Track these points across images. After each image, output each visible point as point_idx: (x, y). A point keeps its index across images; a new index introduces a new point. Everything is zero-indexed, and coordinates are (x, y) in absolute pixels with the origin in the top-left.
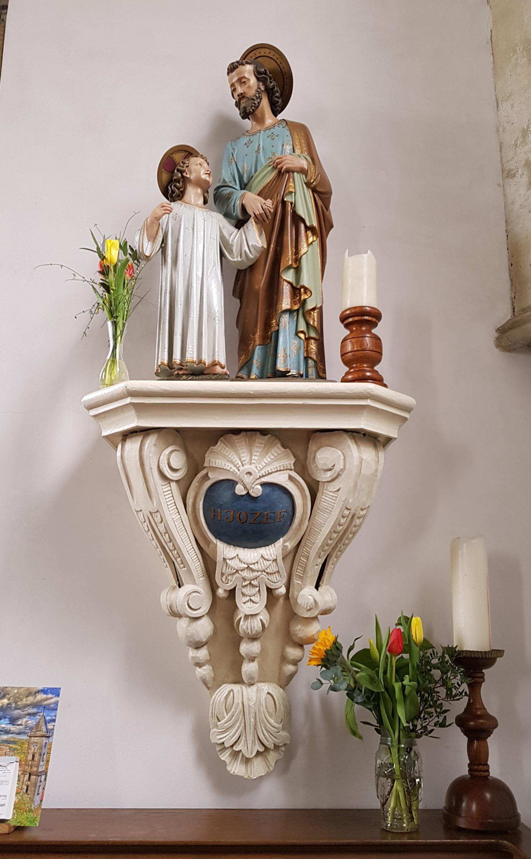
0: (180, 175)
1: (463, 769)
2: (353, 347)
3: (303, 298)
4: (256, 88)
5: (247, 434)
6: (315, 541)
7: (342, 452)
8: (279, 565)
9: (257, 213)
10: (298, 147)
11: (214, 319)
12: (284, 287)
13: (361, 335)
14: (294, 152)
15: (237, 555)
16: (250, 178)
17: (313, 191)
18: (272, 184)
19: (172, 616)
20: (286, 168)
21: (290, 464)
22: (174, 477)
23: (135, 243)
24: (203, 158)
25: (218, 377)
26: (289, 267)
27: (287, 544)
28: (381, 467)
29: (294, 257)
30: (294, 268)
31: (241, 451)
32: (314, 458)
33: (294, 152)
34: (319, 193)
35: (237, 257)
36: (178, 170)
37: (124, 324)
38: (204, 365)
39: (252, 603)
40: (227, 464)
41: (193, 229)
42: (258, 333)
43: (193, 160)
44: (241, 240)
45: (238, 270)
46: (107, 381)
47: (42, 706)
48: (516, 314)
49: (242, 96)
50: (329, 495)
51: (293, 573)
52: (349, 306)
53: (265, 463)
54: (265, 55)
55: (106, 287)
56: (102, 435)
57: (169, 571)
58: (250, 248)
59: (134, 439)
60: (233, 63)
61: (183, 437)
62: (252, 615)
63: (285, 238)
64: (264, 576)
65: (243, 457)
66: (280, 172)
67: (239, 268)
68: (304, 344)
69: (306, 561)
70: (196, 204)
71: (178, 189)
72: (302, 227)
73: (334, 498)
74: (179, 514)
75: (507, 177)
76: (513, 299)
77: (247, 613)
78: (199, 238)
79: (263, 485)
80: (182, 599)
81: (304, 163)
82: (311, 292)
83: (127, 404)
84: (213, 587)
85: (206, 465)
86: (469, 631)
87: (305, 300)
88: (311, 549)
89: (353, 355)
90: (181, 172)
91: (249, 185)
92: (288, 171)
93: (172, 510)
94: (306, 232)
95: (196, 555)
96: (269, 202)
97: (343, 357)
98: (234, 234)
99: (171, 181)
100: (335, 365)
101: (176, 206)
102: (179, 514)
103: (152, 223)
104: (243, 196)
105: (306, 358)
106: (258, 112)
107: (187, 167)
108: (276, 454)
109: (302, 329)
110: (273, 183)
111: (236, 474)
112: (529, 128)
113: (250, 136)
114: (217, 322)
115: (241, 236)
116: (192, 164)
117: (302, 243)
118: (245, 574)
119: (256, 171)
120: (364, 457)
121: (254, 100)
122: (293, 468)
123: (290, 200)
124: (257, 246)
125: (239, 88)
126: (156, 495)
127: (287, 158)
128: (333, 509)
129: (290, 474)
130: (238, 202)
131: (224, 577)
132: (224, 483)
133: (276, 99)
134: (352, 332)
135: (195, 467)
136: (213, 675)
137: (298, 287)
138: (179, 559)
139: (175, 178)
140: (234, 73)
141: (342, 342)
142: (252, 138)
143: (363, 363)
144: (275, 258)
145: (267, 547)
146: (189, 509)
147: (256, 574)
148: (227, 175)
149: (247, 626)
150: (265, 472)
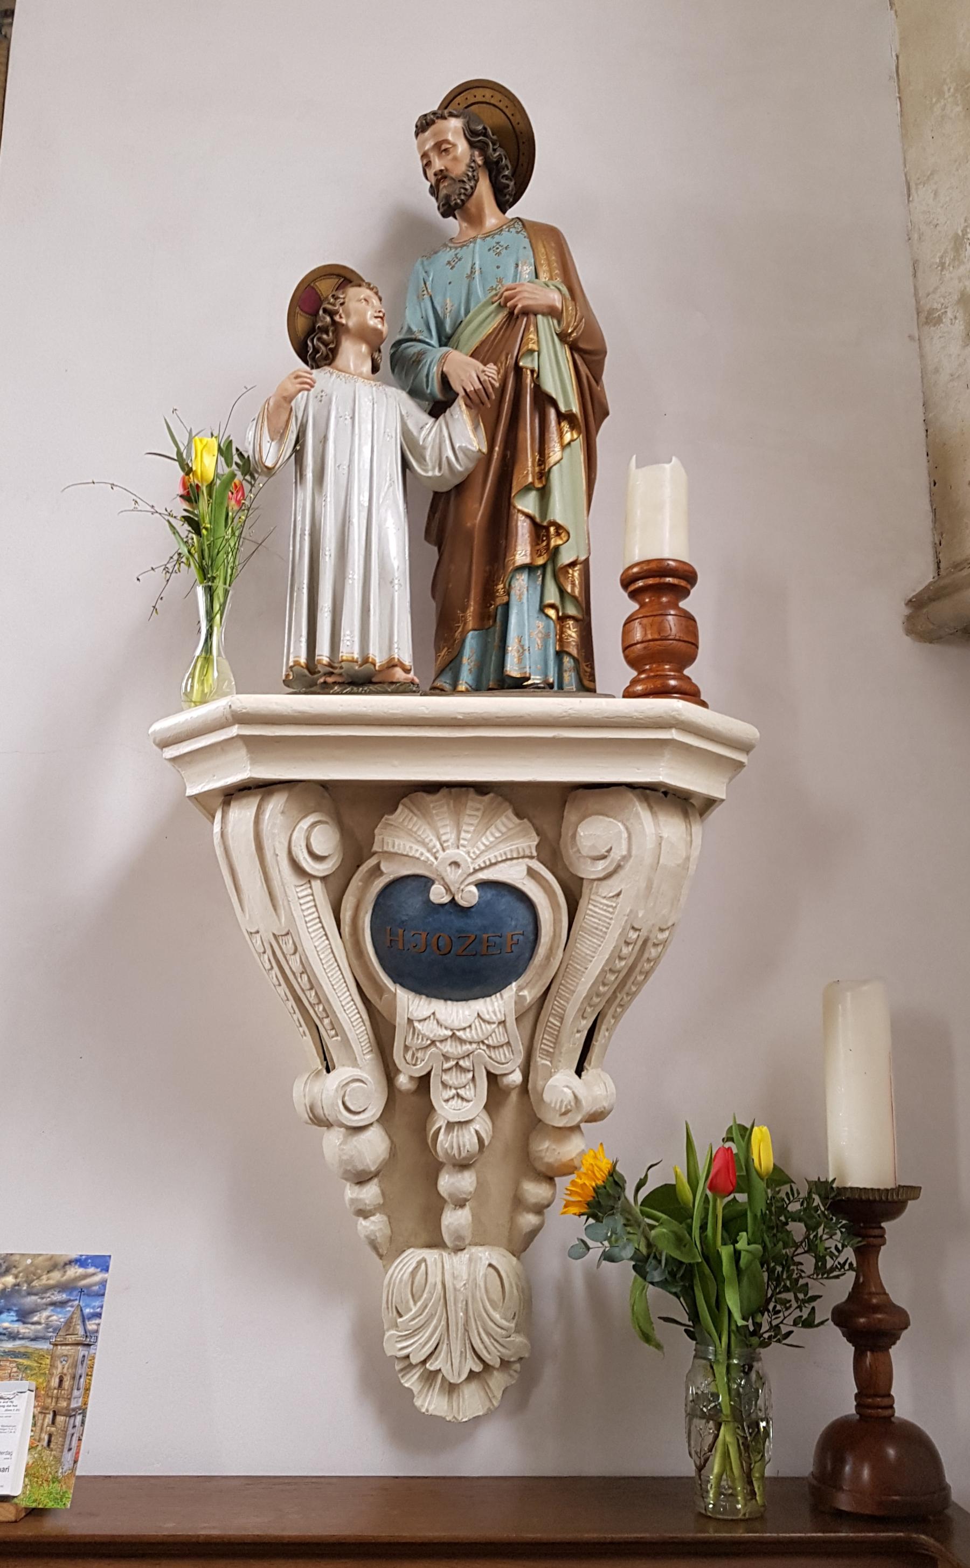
0: (328, 319)
1: (845, 1405)
2: (646, 634)
3: (553, 544)
4: (467, 160)
5: (450, 792)
6: (576, 987)
7: (624, 825)
8: (509, 1031)
9: (470, 388)
10: (545, 268)
11: (391, 582)
12: (519, 523)
13: (660, 612)
14: (537, 277)
15: (434, 1014)
16: (457, 325)
17: (571, 349)
18: (496, 336)
19: (315, 1124)
20: (523, 307)
21: (530, 847)
22: (318, 870)
23: (247, 444)
24: (372, 289)
25: (398, 688)
26: (528, 488)
27: (525, 993)
28: (695, 853)
29: (537, 469)
30: (538, 489)
31: (440, 824)
32: (574, 836)
33: (537, 277)
34: (582, 352)
35: (433, 469)
36: (325, 311)
37: (226, 592)
38: (372, 667)
39: (460, 1101)
40: (415, 847)
41: (353, 418)
42: (472, 608)
43: (352, 291)
44: (440, 439)
45: (436, 493)
46: (196, 696)
47: (77, 1288)
48: (943, 572)
49: (442, 176)
50: (601, 903)
51: (535, 1045)
52: (637, 559)
53: (484, 845)
54: (484, 100)
55: (194, 524)
56: (187, 794)
57: (308, 1042)
58: (457, 452)
59: (244, 801)
60: (425, 115)
61: (334, 798)
62: (459, 1122)
63: (521, 435)
64: (482, 1051)
65: (445, 834)
66: (511, 313)
67: (436, 490)
68: (555, 627)
69: (558, 1024)
70: (358, 372)
71: (326, 344)
72: (552, 414)
73: (611, 910)
74: (328, 939)
75: (927, 323)
76: (937, 546)
77: (452, 1120)
78: (363, 434)
79: (481, 885)
80: (332, 1093)
81: (555, 298)
82: (568, 533)
83: (233, 738)
84: (389, 1072)
85: (376, 848)
86: (856, 1152)
87: (557, 548)
88: (568, 1003)
89: (645, 648)
90: (331, 314)
91: (455, 338)
92: (526, 312)
93: (314, 931)
94: (559, 423)
95: (359, 1013)
96: (491, 369)
97: (627, 651)
98: (427, 426)
99: (312, 331)
100: (612, 667)
101: (321, 376)
102: (328, 939)
103: (278, 406)
104: (444, 357)
105: (559, 654)
106: (471, 205)
107: (342, 304)
108: (504, 830)
109: (552, 601)
110: (498, 334)
111: (431, 865)
112: (967, 233)
113: (456, 248)
114: (396, 587)
115: (441, 431)
116: (350, 300)
117: (552, 444)
118: (448, 1047)
119: (467, 312)
120: (665, 835)
121: (464, 182)
122: (535, 854)
123: (529, 365)
124: (469, 450)
125: (437, 160)
126: (286, 903)
127: (525, 288)
128: (608, 928)
129: (530, 865)
130: (435, 369)
131: (410, 1053)
132: (409, 881)
133: (504, 181)
134: (642, 606)
135: (357, 852)
136: (388, 1232)
137: (545, 524)
138: (326, 1021)
139: (319, 324)
140: (427, 134)
141: (625, 624)
142: (461, 253)
143: (663, 663)
144: (502, 471)
145: (488, 999)
146: (346, 929)
147: (467, 1047)
148: (414, 319)
149: (452, 1143)
150: (484, 862)
